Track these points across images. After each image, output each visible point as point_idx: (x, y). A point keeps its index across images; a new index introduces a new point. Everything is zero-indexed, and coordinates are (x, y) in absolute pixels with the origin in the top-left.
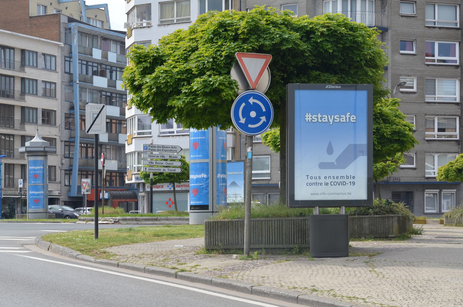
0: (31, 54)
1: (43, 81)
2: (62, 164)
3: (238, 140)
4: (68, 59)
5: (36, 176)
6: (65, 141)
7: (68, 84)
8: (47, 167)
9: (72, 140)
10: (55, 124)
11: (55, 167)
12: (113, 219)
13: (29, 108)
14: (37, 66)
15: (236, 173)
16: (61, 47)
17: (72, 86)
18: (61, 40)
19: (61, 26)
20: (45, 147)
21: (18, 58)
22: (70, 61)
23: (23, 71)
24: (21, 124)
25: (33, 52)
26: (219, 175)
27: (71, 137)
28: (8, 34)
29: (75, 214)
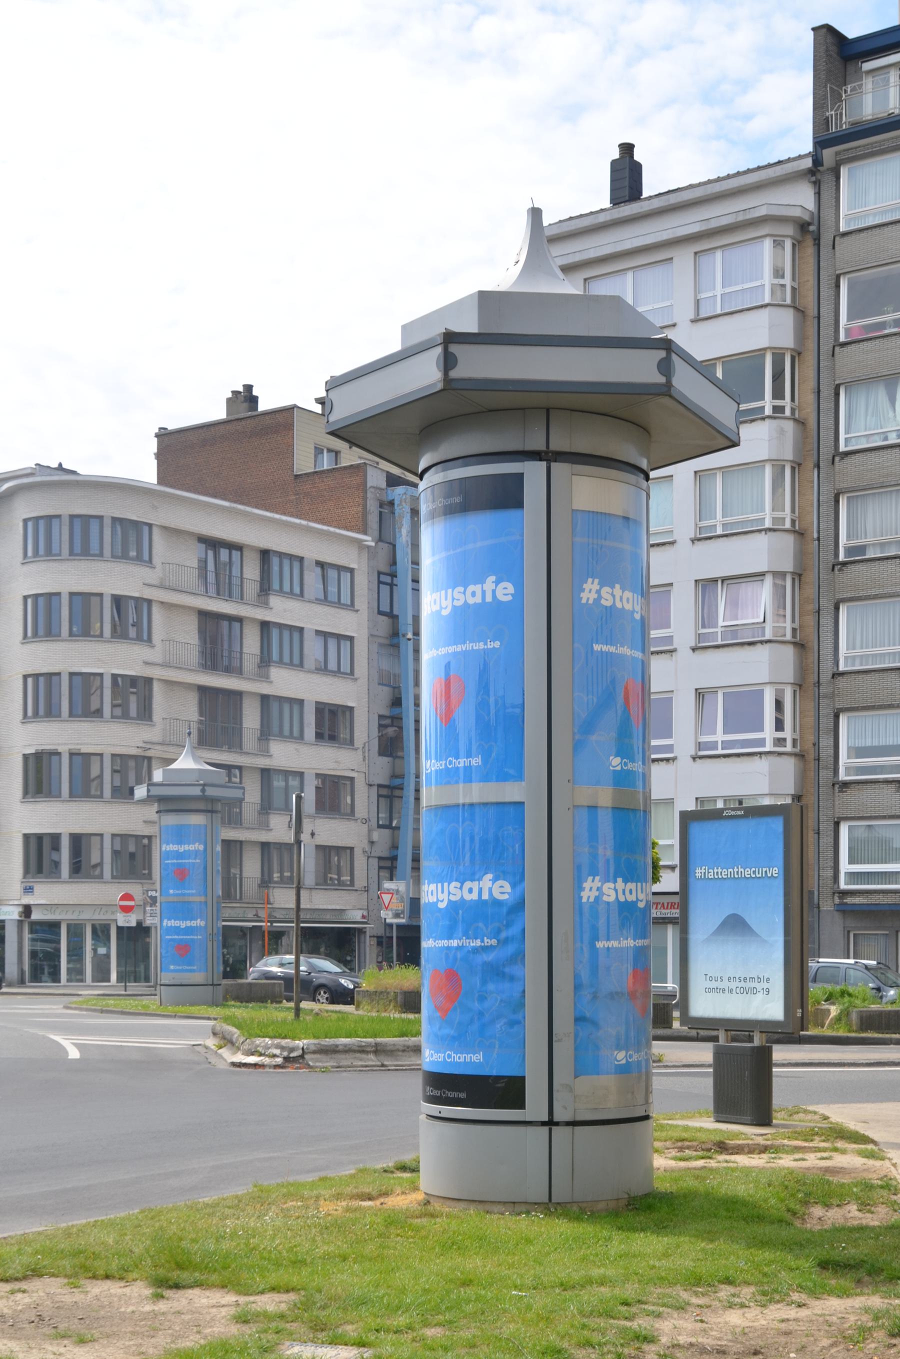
0: (286, 563)
1: (318, 632)
2: (372, 843)
3: (812, 774)
4: (388, 579)
5: (181, 874)
6: (379, 786)
7: (386, 642)
8: (219, 848)
9: (397, 782)
10: (351, 742)
11: (352, 849)
12: (283, 1048)
13: (281, 699)
14: (302, 594)
15: (748, 872)
16: (368, 547)
17: (396, 646)
18: (369, 531)
19: (369, 495)
20: (204, 785)
21: (252, 571)
22: (392, 585)
23: (265, 605)
24: (259, 740)
25: (291, 557)
26: (590, 889)
27: (394, 776)
28: (223, 508)
29: (343, 981)
